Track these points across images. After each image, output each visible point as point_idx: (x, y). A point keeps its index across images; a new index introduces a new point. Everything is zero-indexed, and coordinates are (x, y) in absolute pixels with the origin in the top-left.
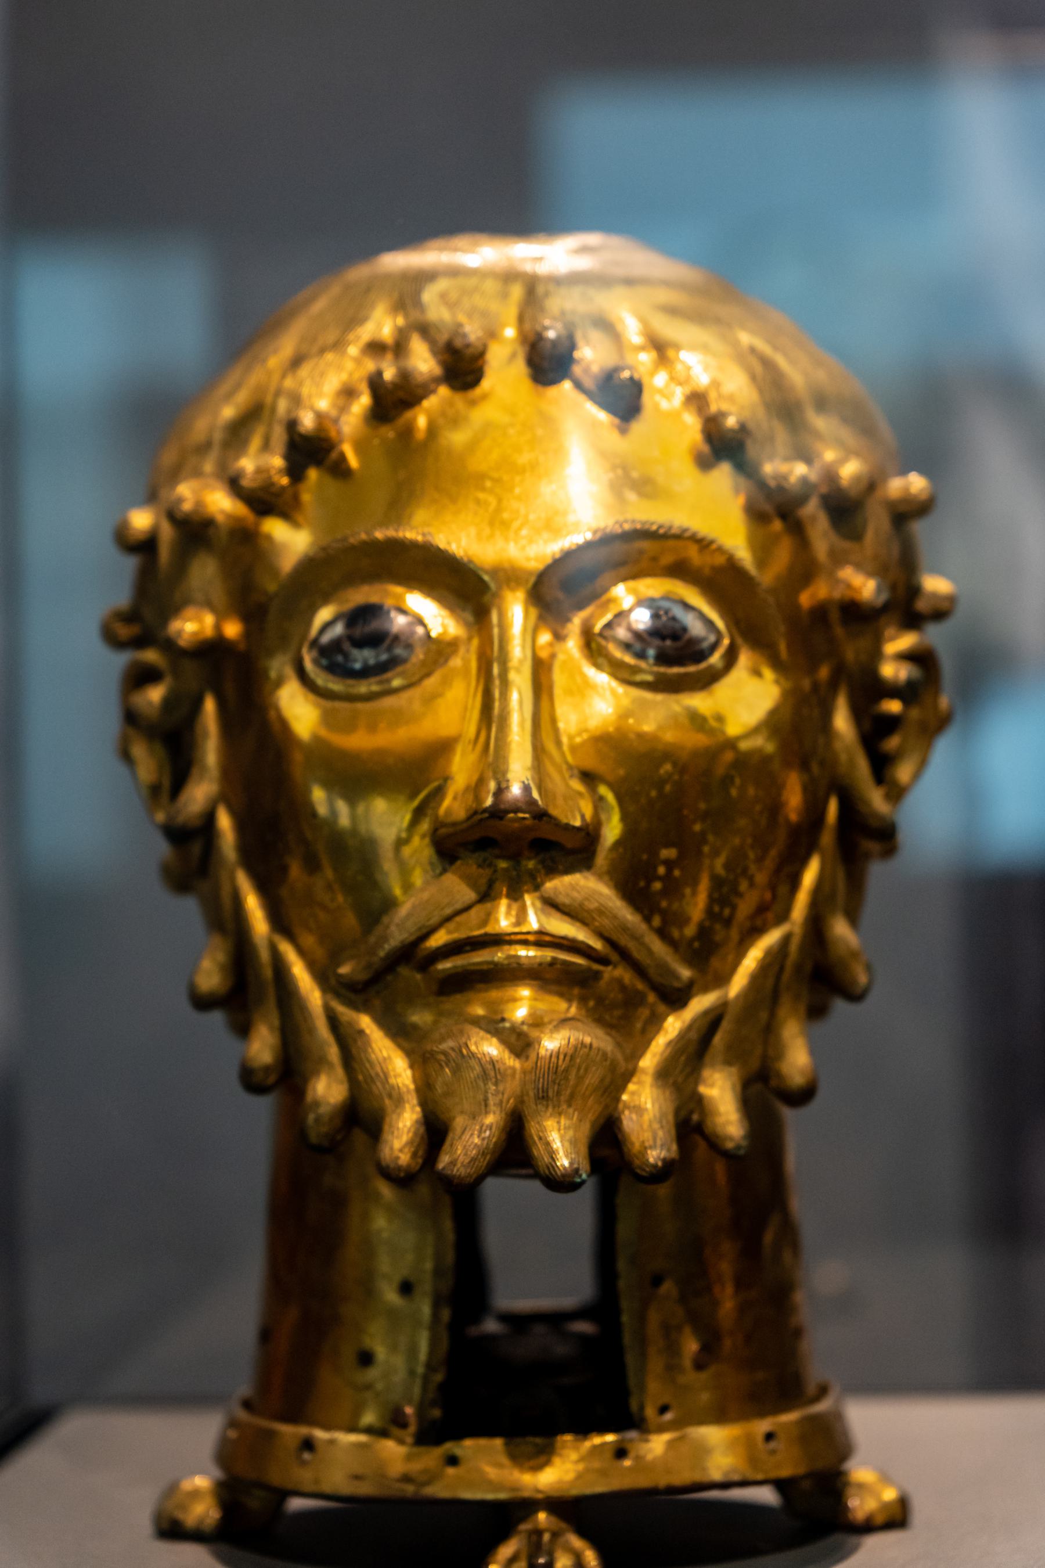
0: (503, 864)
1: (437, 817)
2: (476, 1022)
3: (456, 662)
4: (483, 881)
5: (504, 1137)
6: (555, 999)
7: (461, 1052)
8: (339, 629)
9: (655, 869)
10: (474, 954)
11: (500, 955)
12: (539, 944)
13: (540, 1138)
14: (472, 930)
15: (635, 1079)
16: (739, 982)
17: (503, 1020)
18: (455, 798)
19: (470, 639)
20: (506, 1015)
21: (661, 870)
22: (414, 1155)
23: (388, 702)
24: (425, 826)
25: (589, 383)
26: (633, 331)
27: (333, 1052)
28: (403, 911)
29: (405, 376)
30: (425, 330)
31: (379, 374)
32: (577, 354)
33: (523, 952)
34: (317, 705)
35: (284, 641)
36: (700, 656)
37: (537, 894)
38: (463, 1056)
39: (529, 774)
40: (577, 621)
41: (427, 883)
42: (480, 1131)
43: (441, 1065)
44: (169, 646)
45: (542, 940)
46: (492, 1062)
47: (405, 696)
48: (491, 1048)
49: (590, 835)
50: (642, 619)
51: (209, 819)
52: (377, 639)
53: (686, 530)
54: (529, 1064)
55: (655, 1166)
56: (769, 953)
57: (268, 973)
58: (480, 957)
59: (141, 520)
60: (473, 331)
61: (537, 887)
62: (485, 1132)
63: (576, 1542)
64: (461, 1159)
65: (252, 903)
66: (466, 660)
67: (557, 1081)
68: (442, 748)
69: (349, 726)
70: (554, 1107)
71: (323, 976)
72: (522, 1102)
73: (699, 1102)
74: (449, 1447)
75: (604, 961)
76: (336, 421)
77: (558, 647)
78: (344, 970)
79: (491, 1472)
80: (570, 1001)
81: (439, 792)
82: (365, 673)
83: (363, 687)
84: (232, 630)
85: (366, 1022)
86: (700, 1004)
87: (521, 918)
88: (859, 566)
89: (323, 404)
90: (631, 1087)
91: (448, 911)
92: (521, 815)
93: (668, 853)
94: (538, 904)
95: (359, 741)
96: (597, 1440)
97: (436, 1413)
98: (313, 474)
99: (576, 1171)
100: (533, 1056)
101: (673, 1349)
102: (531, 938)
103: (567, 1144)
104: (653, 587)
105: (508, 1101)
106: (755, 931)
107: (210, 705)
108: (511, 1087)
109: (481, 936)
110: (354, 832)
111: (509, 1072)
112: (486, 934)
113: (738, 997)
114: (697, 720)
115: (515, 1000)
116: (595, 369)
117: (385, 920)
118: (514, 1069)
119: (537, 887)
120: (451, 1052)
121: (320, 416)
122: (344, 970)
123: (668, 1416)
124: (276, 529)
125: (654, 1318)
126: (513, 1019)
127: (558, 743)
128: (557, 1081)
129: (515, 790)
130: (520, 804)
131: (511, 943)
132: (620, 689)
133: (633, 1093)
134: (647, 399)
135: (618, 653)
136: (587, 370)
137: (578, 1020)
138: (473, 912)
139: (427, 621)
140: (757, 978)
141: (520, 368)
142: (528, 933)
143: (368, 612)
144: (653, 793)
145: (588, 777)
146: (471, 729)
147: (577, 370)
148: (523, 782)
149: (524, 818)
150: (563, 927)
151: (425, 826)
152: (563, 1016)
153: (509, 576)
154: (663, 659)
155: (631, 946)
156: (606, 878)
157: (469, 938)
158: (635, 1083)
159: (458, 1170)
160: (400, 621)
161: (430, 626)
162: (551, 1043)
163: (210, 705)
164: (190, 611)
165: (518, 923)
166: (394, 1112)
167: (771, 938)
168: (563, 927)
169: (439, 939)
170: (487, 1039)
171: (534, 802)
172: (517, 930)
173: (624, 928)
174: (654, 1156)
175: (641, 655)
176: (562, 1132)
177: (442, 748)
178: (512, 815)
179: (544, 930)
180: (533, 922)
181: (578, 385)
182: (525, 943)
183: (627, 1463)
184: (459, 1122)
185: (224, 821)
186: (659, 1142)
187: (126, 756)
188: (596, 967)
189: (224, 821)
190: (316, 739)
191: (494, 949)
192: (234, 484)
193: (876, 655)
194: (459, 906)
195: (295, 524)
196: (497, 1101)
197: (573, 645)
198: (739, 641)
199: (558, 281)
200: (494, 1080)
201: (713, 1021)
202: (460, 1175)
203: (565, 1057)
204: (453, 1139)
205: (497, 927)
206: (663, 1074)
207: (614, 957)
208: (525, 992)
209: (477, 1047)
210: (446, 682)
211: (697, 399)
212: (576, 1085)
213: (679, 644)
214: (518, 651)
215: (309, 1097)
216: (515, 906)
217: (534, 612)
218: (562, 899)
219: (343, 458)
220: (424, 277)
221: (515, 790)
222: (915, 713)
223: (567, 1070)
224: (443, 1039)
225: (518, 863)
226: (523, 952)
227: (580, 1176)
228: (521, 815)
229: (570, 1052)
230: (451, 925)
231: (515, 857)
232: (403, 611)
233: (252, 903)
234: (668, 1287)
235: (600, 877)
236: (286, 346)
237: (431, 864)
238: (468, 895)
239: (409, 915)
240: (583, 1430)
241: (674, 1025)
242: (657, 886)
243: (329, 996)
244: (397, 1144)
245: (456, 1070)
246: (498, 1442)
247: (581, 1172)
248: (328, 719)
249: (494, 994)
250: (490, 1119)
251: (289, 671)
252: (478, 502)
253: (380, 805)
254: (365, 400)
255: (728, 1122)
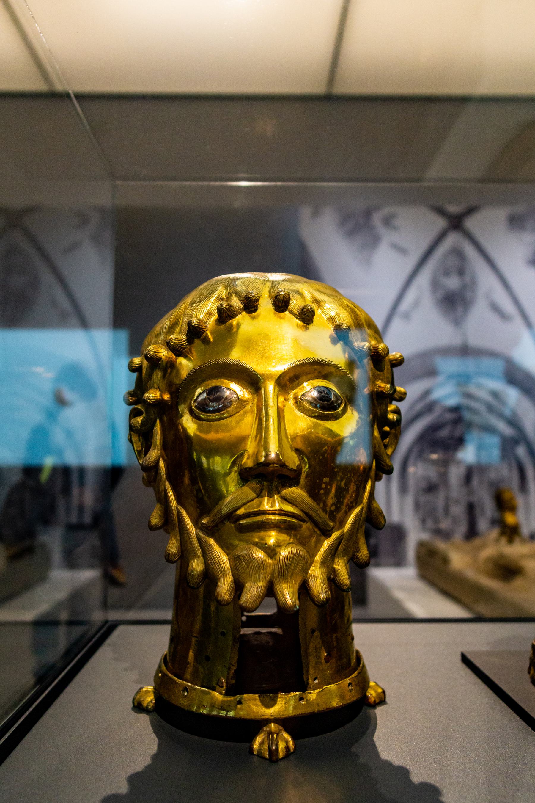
0: (266, 484)
1: (241, 465)
2: (256, 544)
3: (248, 407)
4: (258, 490)
5: (266, 591)
6: (285, 536)
7: (249, 556)
8: (205, 395)
9: (321, 485)
10: (254, 518)
11: (265, 518)
12: (279, 514)
13: (280, 592)
14: (254, 508)
15: (313, 565)
16: (348, 526)
17: (266, 544)
18: (248, 458)
19: (253, 399)
20: (267, 542)
21: (324, 486)
22: (230, 596)
23: (222, 422)
24: (236, 468)
25: (295, 312)
26: (308, 296)
27: (199, 551)
28: (228, 500)
29: (230, 307)
30: (237, 293)
31: (221, 305)
32: (291, 302)
33: (271, 517)
34: (196, 423)
35: (185, 400)
36: (335, 408)
37: (279, 495)
38: (250, 558)
39: (277, 449)
40: (292, 394)
41: (236, 490)
42: (257, 589)
43: (241, 561)
44: (144, 402)
45: (281, 512)
46: (262, 561)
47: (229, 420)
48: (260, 554)
49: (298, 472)
50: (315, 394)
51: (158, 462)
52: (218, 399)
53: (331, 362)
54: (276, 562)
55: (323, 601)
56: (357, 515)
57: (176, 520)
58: (258, 519)
59: (137, 360)
60: (254, 292)
61: (279, 493)
62: (259, 589)
63: (286, 735)
64: (250, 600)
65: (171, 493)
66: (253, 407)
67: (287, 569)
68: (243, 439)
69: (208, 432)
70: (286, 579)
71: (196, 522)
72: (273, 577)
73: (334, 570)
74: (238, 697)
75: (303, 521)
76: (206, 323)
77: (286, 403)
78: (204, 521)
79: (255, 708)
80: (290, 536)
81: (242, 455)
82: (214, 411)
83: (213, 416)
84: (166, 397)
85: (212, 541)
86: (335, 535)
87: (273, 505)
88: (382, 380)
89: (201, 317)
90: (312, 568)
91: (245, 501)
92: (276, 465)
93: (326, 480)
94: (279, 499)
95: (212, 436)
96: (292, 694)
97: (233, 682)
98: (197, 341)
99: (295, 606)
100: (277, 558)
101: (318, 657)
102: (277, 512)
103: (291, 595)
104: (321, 383)
105: (268, 577)
106: (351, 508)
107: (158, 423)
108: (269, 570)
109: (258, 511)
110: (209, 469)
111: (268, 565)
112: (260, 510)
113: (347, 531)
114: (330, 432)
115: (270, 536)
116: (297, 307)
117: (220, 503)
118: (270, 563)
119: (279, 493)
120: (245, 556)
121: (199, 320)
122: (204, 521)
123: (316, 682)
124: (182, 361)
125: (312, 645)
126: (269, 543)
127: (287, 438)
128: (287, 569)
129: (273, 456)
130: (275, 461)
131: (269, 514)
132: (308, 418)
133: (313, 571)
134: (315, 318)
135: (307, 405)
136: (294, 307)
137: (294, 543)
138: (254, 501)
139: (237, 392)
140: (353, 525)
141: (271, 307)
142: (276, 510)
143: (216, 389)
144: (321, 457)
145: (298, 451)
146: (253, 432)
147: (290, 307)
148: (276, 452)
149: (276, 466)
150: (289, 508)
151: (236, 468)
152: (288, 542)
153: (269, 377)
154: (323, 408)
155: (314, 515)
156: (304, 489)
157: (253, 512)
158: (313, 567)
159: (248, 605)
160: (227, 393)
161: (239, 395)
162: (284, 553)
163: (158, 423)
164: (152, 391)
165: (272, 507)
166: (222, 577)
167: (357, 511)
168: (289, 508)
169: (241, 511)
170: (260, 552)
171: (280, 460)
172: (271, 509)
173: (311, 508)
174: (322, 596)
175: (316, 407)
176: (289, 589)
177: (243, 439)
178: (272, 465)
179: (282, 509)
180: (277, 507)
181: (291, 312)
182: (274, 514)
183: (303, 703)
184: (248, 585)
185: (162, 464)
186: (324, 591)
187: (131, 441)
188: (301, 523)
189: (162, 464)
190: (195, 434)
191: (263, 516)
192: (169, 345)
193: (386, 412)
194: (249, 499)
195: (189, 360)
196: (264, 577)
197: (291, 402)
198: (348, 403)
199: (279, 283)
200: (262, 568)
201: (339, 540)
202: (249, 608)
203: (290, 559)
204: (246, 592)
205: (264, 508)
206: (323, 563)
207: (306, 519)
208: (273, 533)
209: (256, 555)
210: (245, 413)
211: (331, 319)
212: (294, 570)
213: (329, 403)
214: (271, 402)
215: (190, 568)
216: (271, 500)
217: (277, 388)
218: (288, 497)
219: (207, 337)
220: (235, 280)
221: (273, 456)
222: (393, 431)
223: (290, 564)
224: (242, 551)
225: (272, 483)
226: (271, 517)
227: (296, 607)
228: (276, 465)
229: (292, 557)
230: (246, 506)
231: (271, 482)
232: (229, 389)
233: (171, 493)
234: (316, 633)
235: (301, 489)
236: (189, 299)
237: (238, 482)
238: (254, 495)
239: (230, 502)
240: (287, 691)
241: (327, 544)
242: (322, 492)
243: (198, 530)
244: (224, 591)
245: (248, 563)
246: (257, 696)
247: (297, 606)
248: (199, 429)
249: (262, 534)
250: (260, 584)
251: (186, 410)
252: (256, 350)
253: (217, 459)
254: (215, 317)
255: (345, 579)
